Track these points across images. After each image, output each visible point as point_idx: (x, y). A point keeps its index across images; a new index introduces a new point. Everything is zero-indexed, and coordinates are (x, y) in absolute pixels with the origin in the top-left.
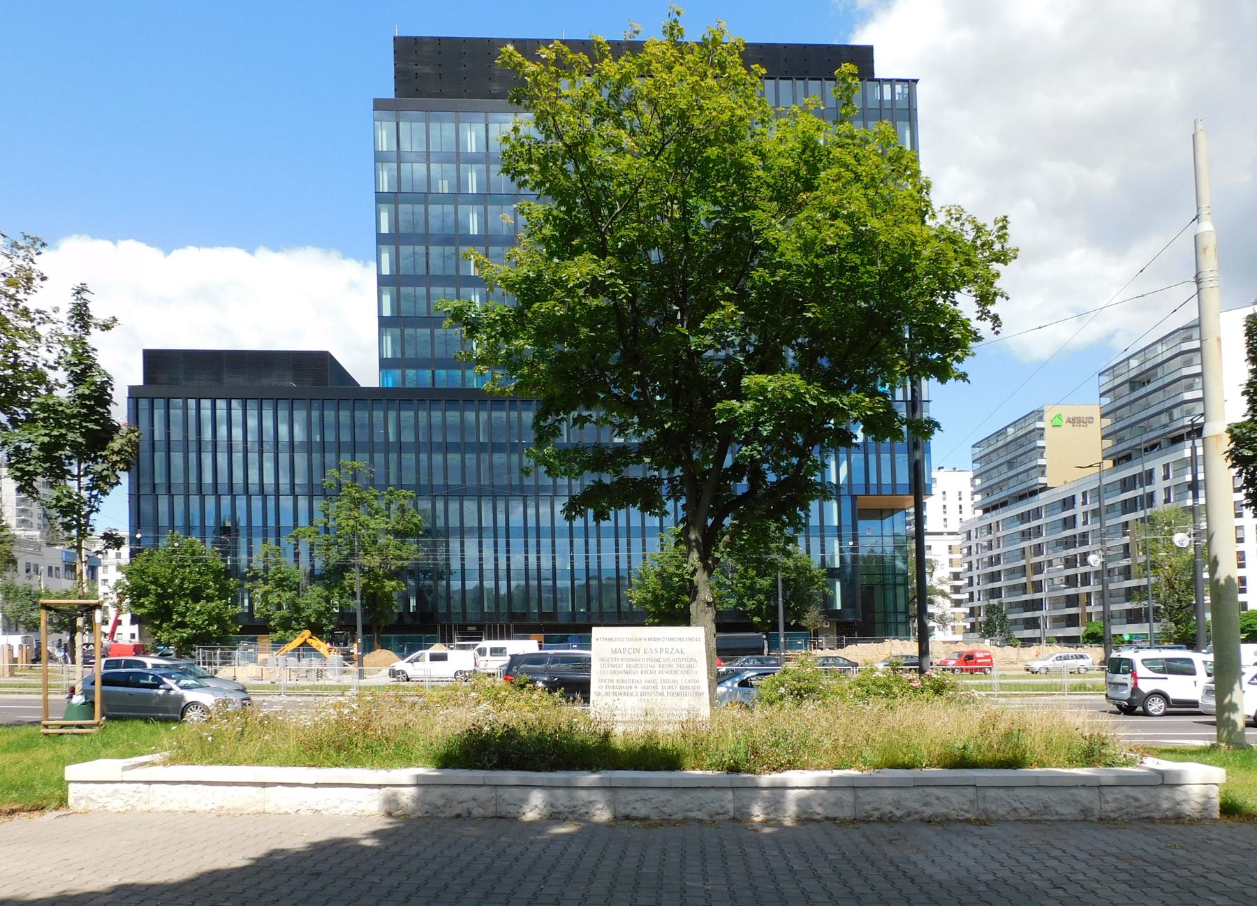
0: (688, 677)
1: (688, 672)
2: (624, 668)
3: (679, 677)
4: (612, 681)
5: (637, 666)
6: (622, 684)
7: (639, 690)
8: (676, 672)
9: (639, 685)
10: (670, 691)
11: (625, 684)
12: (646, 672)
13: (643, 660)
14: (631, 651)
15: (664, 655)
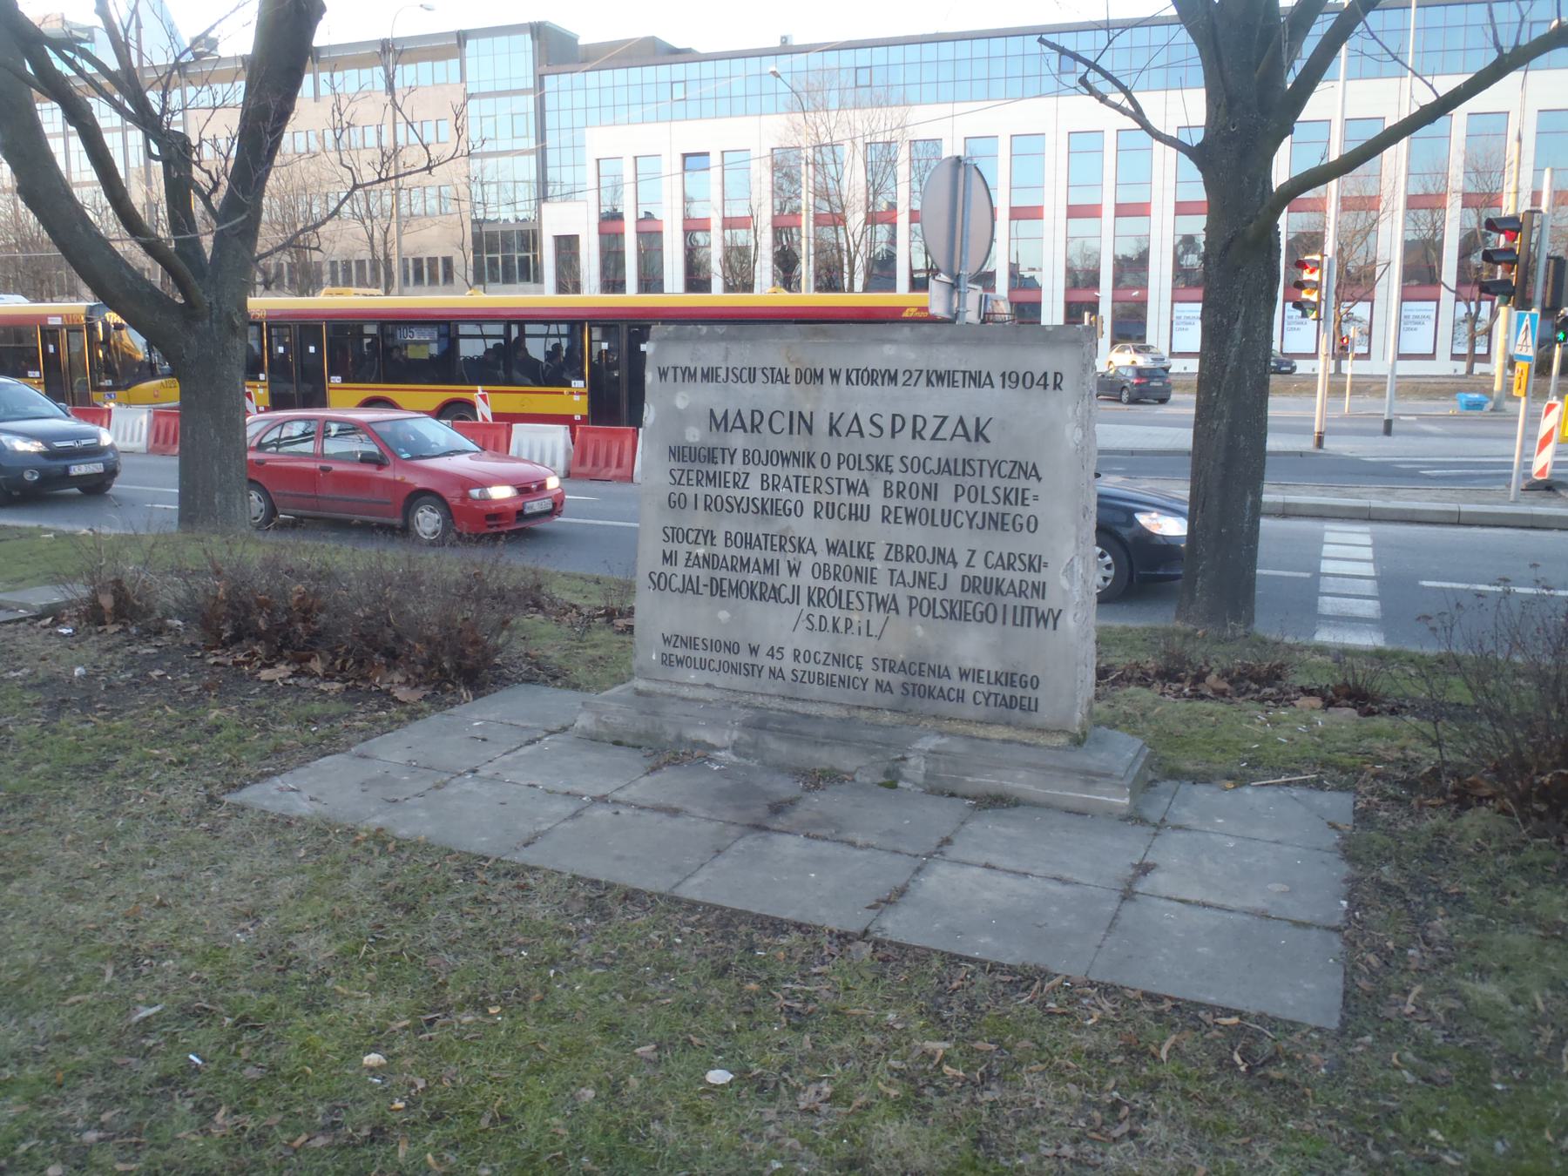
0: (1004, 543)
1: (996, 522)
2: (754, 489)
3: (958, 540)
4: (709, 536)
5: (799, 484)
6: (745, 553)
7: (805, 579)
8: (949, 518)
9: (807, 560)
10: (919, 592)
11: (754, 554)
12: (832, 511)
13: (826, 460)
14: (781, 423)
15: (905, 445)
